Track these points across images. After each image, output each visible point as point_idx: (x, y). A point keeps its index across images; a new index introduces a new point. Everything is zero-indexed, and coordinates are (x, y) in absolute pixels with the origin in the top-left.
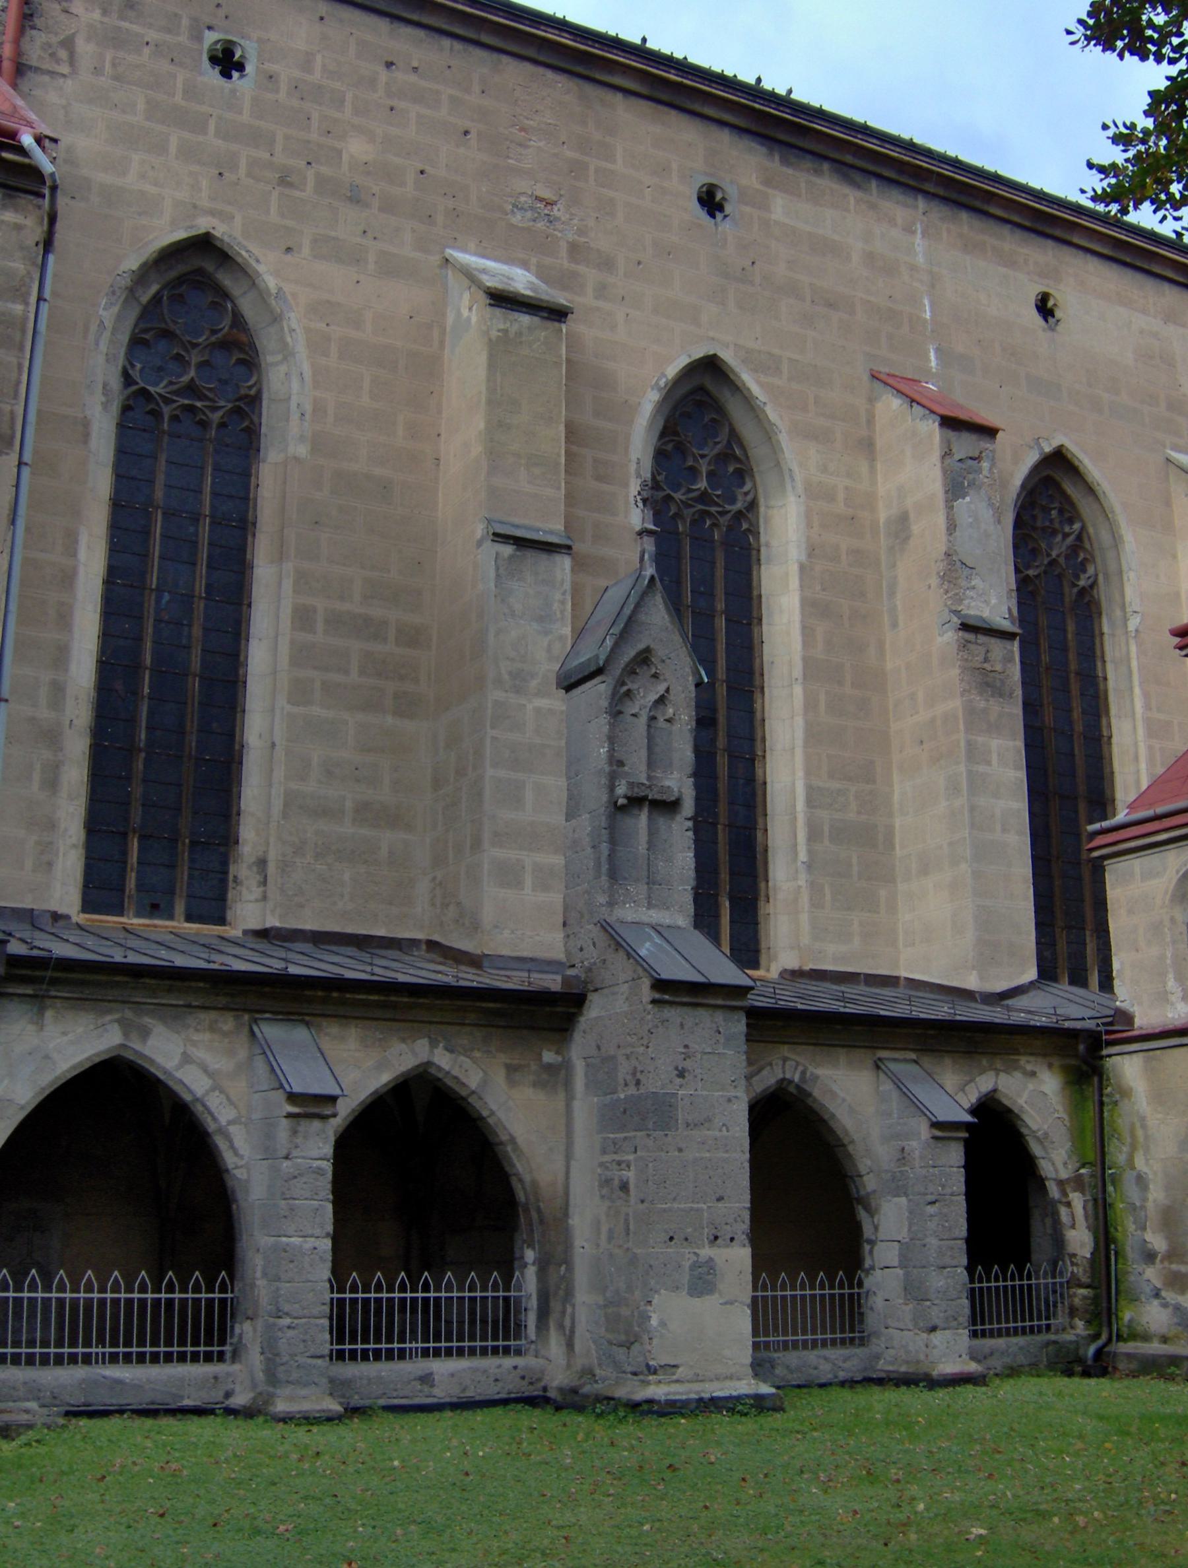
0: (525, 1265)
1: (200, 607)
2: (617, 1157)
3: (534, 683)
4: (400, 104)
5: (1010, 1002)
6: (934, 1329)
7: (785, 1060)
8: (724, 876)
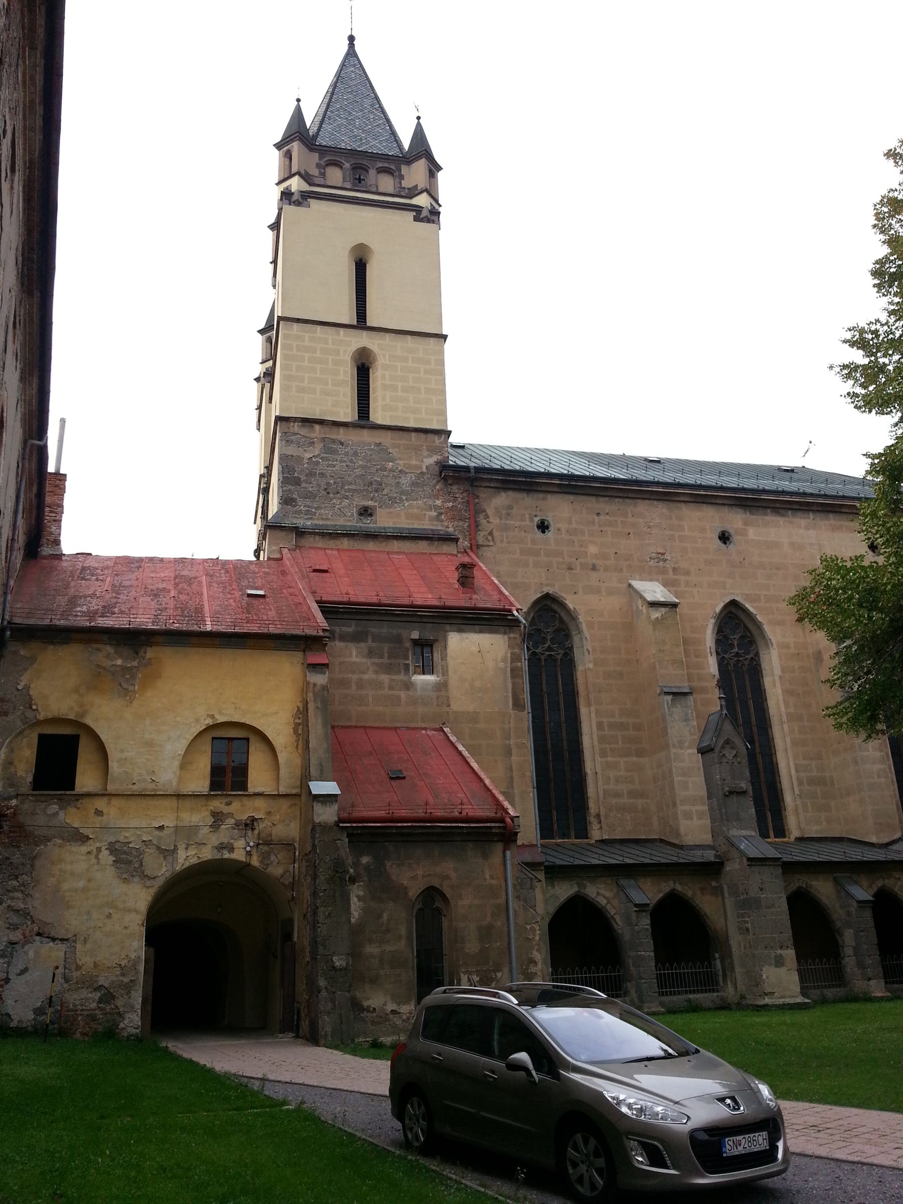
0: (716, 959)
1: (564, 725)
2: (743, 919)
3: (686, 744)
4: (604, 529)
5: (890, 847)
6: (870, 979)
7: (799, 879)
8: (766, 802)
